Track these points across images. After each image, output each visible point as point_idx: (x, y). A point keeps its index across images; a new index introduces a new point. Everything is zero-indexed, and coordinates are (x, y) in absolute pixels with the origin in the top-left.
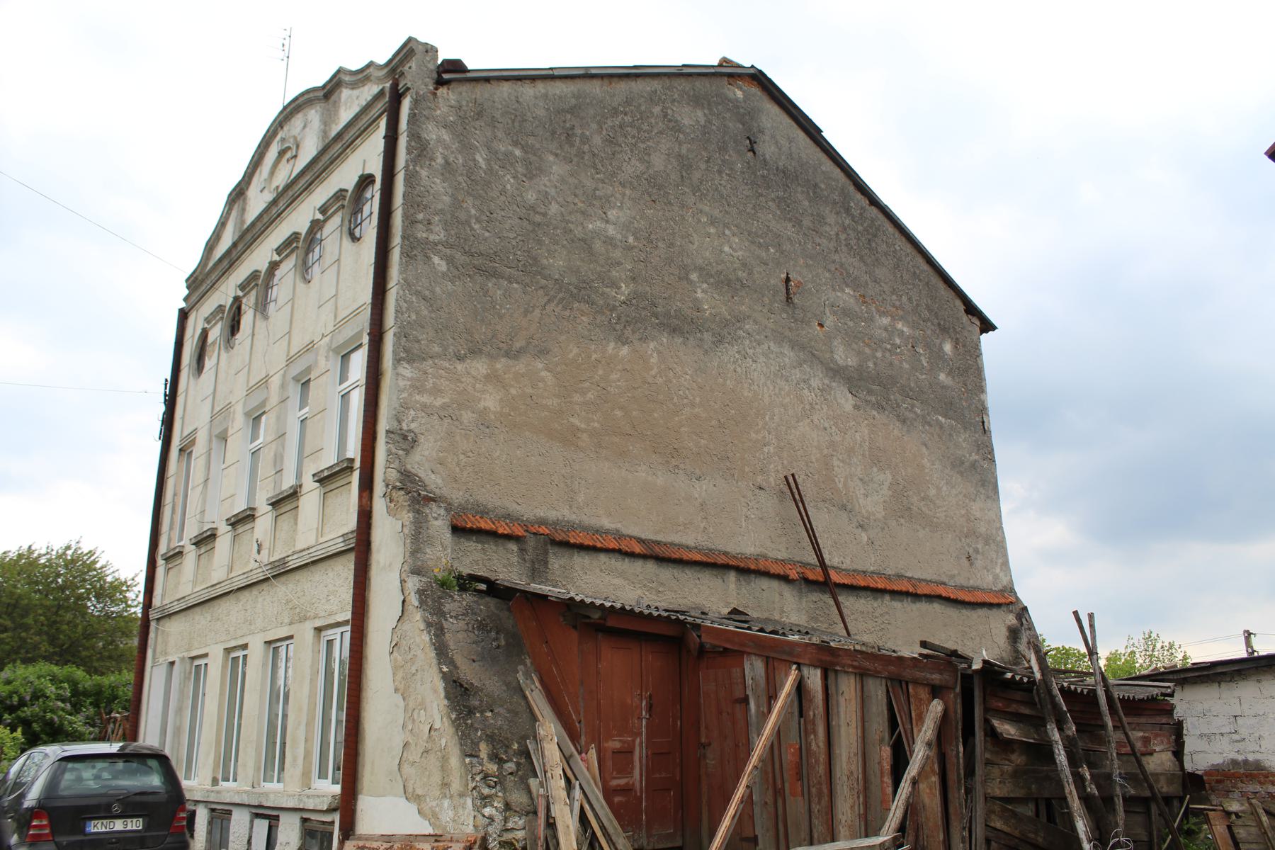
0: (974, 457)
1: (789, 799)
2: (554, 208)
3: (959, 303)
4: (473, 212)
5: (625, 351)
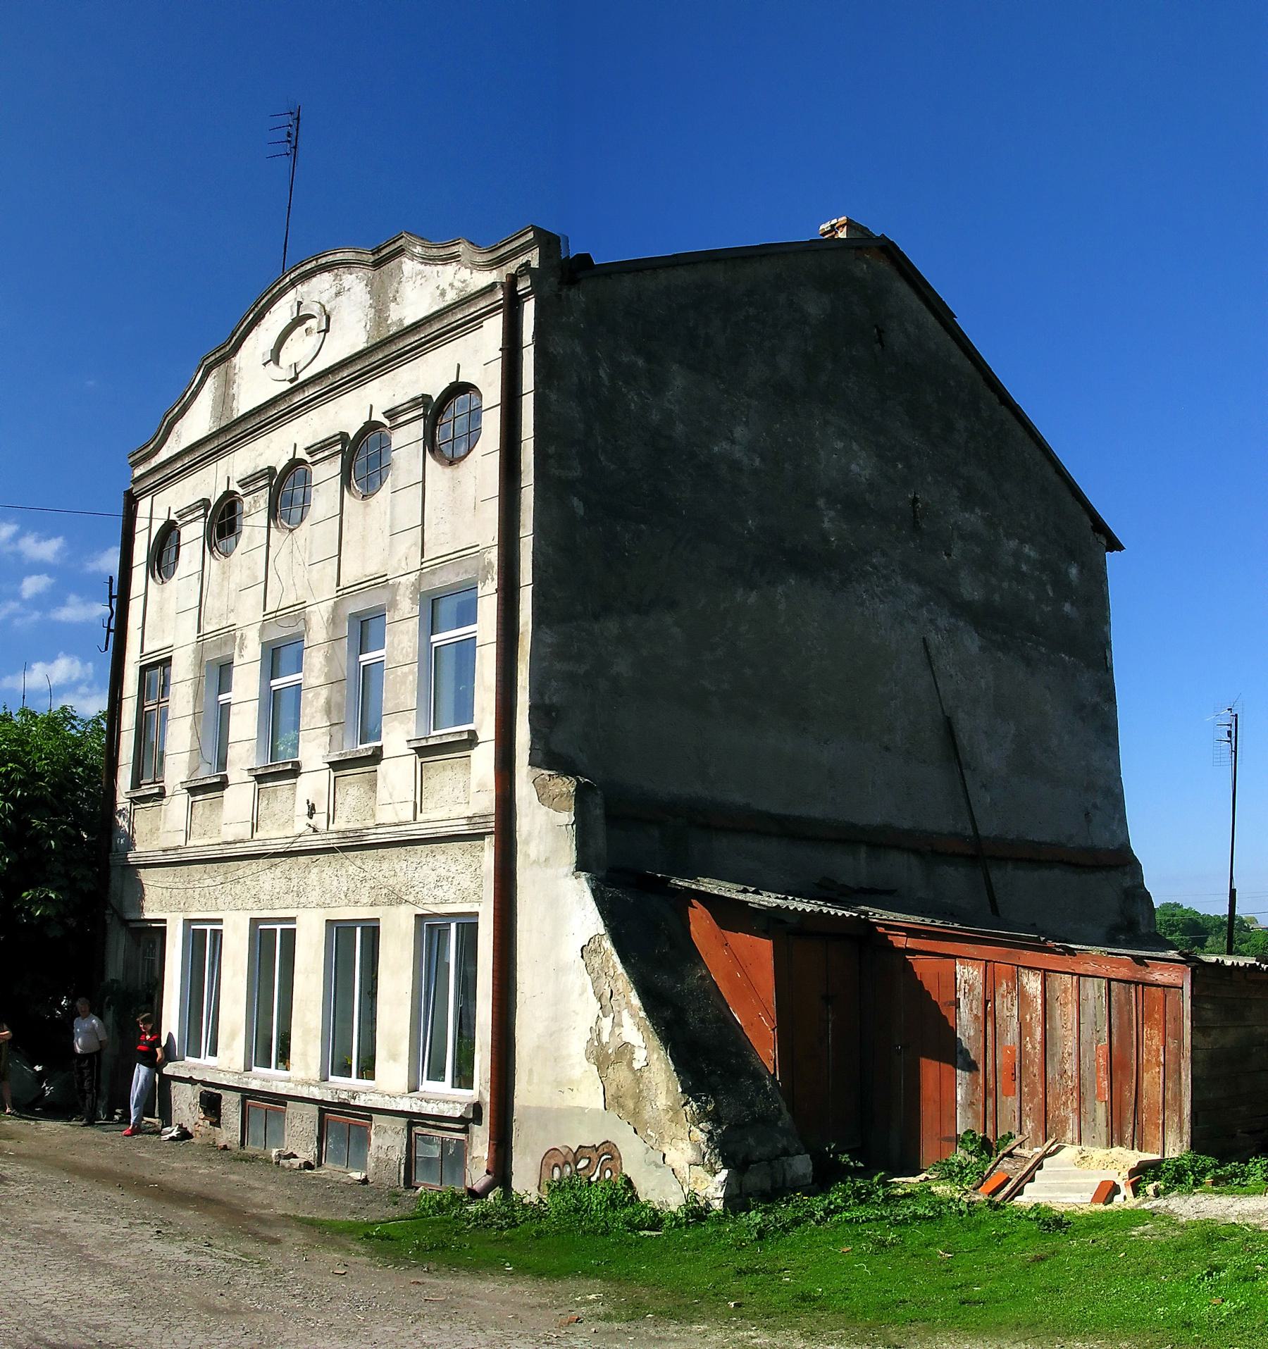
0: (1097, 699)
1: (1001, 1098)
2: (680, 428)
3: (1086, 518)
4: (600, 440)
5: (753, 598)
